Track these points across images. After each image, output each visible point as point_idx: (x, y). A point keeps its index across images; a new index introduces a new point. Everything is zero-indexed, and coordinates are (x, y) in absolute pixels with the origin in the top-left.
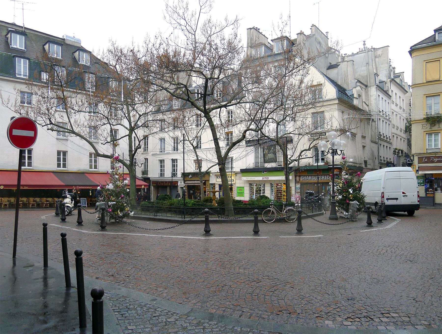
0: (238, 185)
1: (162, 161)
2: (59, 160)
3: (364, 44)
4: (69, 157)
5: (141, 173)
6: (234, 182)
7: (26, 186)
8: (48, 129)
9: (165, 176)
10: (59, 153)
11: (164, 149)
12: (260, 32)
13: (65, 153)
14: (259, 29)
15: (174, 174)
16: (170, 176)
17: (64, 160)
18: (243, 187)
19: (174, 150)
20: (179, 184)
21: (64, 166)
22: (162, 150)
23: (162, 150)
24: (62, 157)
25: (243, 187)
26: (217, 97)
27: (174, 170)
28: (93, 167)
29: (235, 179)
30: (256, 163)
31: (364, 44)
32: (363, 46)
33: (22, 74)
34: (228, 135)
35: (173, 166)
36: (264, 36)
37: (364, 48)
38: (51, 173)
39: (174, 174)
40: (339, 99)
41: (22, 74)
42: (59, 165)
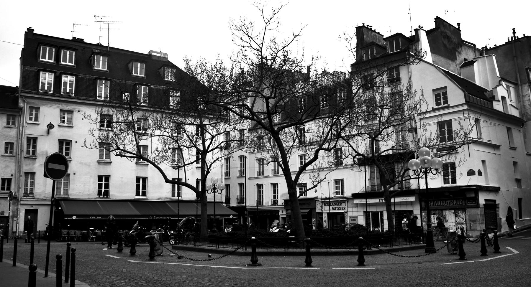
0: (350, 214)
1: (260, 186)
2: (138, 187)
3: (514, 33)
4: (112, 182)
5: (236, 201)
6: (346, 211)
7: (99, 216)
8: (117, 155)
9: (264, 204)
10: (138, 179)
11: (263, 171)
12: (373, 29)
13: (145, 179)
14: (371, 27)
15: (275, 202)
16: (256, 205)
17: (144, 187)
18: (357, 217)
19: (275, 173)
20: (280, 213)
21: (144, 194)
22: (261, 173)
23: (261, 173)
24: (103, 183)
25: (357, 217)
26: (323, 107)
27: (274, 197)
28: (141, 194)
29: (346, 207)
30: (372, 186)
31: (514, 33)
32: (513, 35)
33: (103, 96)
34: (337, 153)
35: (274, 192)
36: (379, 33)
37: (514, 36)
38: (129, 203)
39: (275, 202)
40: (467, 103)
41: (103, 96)
42: (138, 194)
